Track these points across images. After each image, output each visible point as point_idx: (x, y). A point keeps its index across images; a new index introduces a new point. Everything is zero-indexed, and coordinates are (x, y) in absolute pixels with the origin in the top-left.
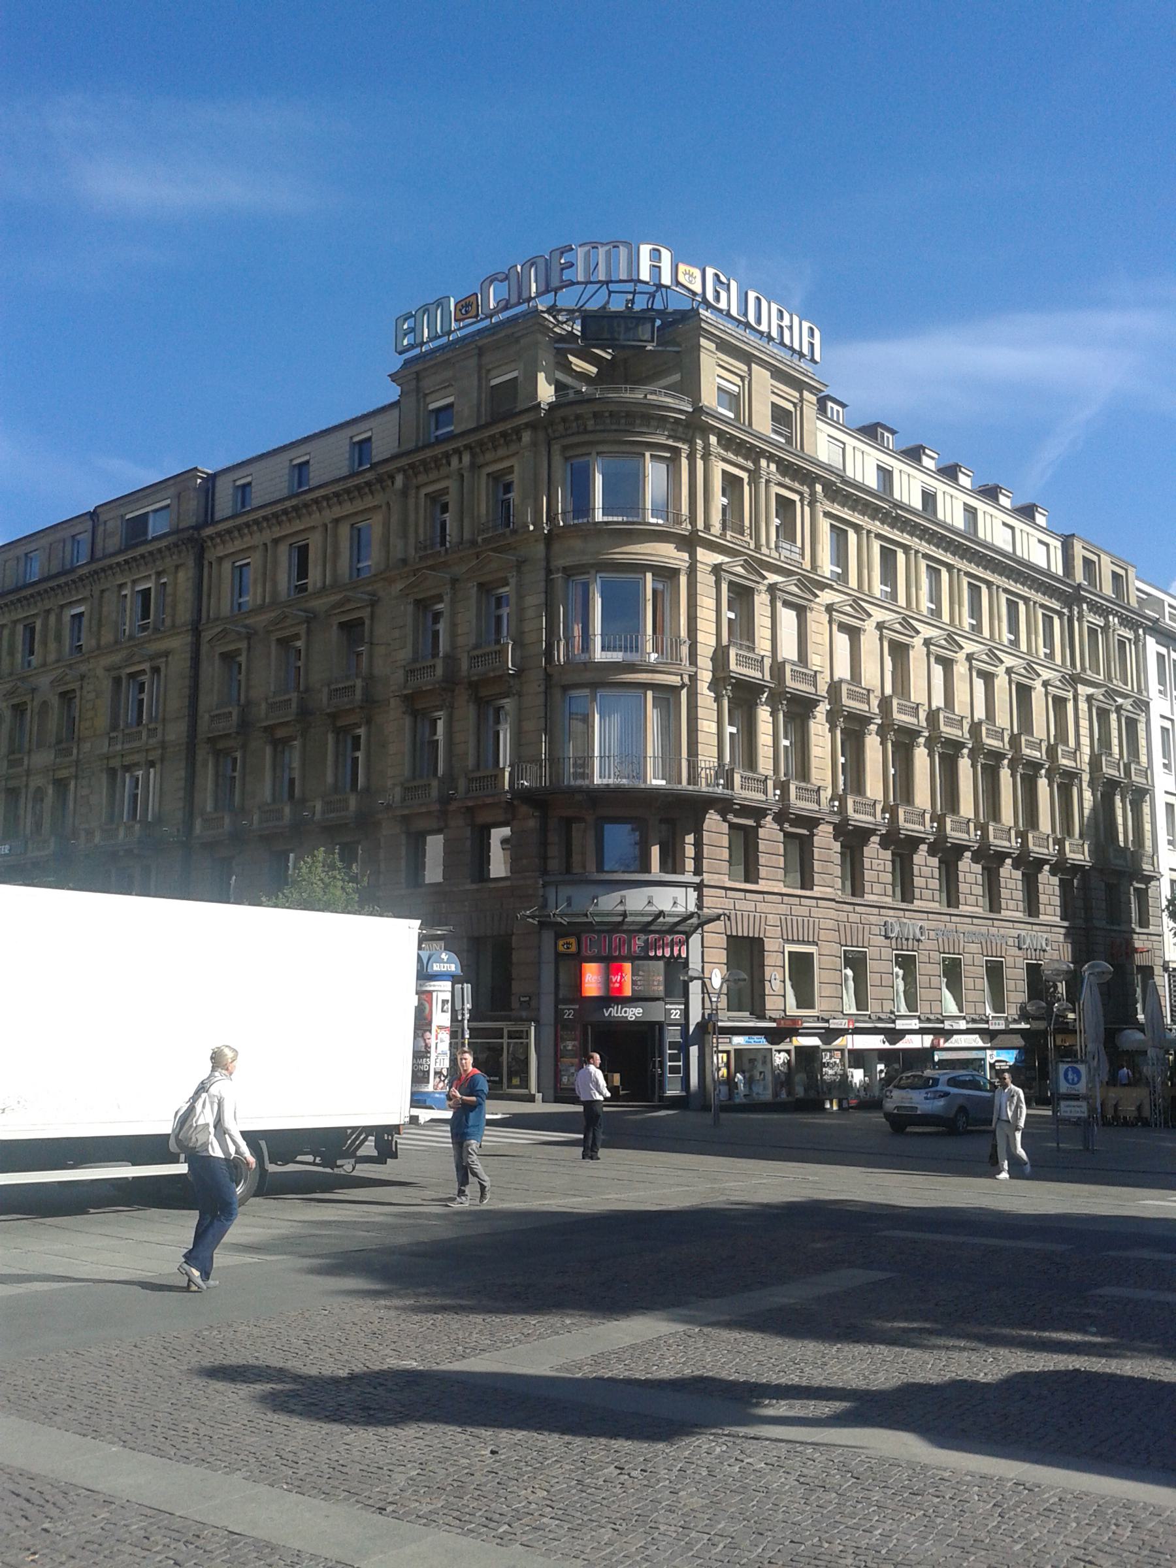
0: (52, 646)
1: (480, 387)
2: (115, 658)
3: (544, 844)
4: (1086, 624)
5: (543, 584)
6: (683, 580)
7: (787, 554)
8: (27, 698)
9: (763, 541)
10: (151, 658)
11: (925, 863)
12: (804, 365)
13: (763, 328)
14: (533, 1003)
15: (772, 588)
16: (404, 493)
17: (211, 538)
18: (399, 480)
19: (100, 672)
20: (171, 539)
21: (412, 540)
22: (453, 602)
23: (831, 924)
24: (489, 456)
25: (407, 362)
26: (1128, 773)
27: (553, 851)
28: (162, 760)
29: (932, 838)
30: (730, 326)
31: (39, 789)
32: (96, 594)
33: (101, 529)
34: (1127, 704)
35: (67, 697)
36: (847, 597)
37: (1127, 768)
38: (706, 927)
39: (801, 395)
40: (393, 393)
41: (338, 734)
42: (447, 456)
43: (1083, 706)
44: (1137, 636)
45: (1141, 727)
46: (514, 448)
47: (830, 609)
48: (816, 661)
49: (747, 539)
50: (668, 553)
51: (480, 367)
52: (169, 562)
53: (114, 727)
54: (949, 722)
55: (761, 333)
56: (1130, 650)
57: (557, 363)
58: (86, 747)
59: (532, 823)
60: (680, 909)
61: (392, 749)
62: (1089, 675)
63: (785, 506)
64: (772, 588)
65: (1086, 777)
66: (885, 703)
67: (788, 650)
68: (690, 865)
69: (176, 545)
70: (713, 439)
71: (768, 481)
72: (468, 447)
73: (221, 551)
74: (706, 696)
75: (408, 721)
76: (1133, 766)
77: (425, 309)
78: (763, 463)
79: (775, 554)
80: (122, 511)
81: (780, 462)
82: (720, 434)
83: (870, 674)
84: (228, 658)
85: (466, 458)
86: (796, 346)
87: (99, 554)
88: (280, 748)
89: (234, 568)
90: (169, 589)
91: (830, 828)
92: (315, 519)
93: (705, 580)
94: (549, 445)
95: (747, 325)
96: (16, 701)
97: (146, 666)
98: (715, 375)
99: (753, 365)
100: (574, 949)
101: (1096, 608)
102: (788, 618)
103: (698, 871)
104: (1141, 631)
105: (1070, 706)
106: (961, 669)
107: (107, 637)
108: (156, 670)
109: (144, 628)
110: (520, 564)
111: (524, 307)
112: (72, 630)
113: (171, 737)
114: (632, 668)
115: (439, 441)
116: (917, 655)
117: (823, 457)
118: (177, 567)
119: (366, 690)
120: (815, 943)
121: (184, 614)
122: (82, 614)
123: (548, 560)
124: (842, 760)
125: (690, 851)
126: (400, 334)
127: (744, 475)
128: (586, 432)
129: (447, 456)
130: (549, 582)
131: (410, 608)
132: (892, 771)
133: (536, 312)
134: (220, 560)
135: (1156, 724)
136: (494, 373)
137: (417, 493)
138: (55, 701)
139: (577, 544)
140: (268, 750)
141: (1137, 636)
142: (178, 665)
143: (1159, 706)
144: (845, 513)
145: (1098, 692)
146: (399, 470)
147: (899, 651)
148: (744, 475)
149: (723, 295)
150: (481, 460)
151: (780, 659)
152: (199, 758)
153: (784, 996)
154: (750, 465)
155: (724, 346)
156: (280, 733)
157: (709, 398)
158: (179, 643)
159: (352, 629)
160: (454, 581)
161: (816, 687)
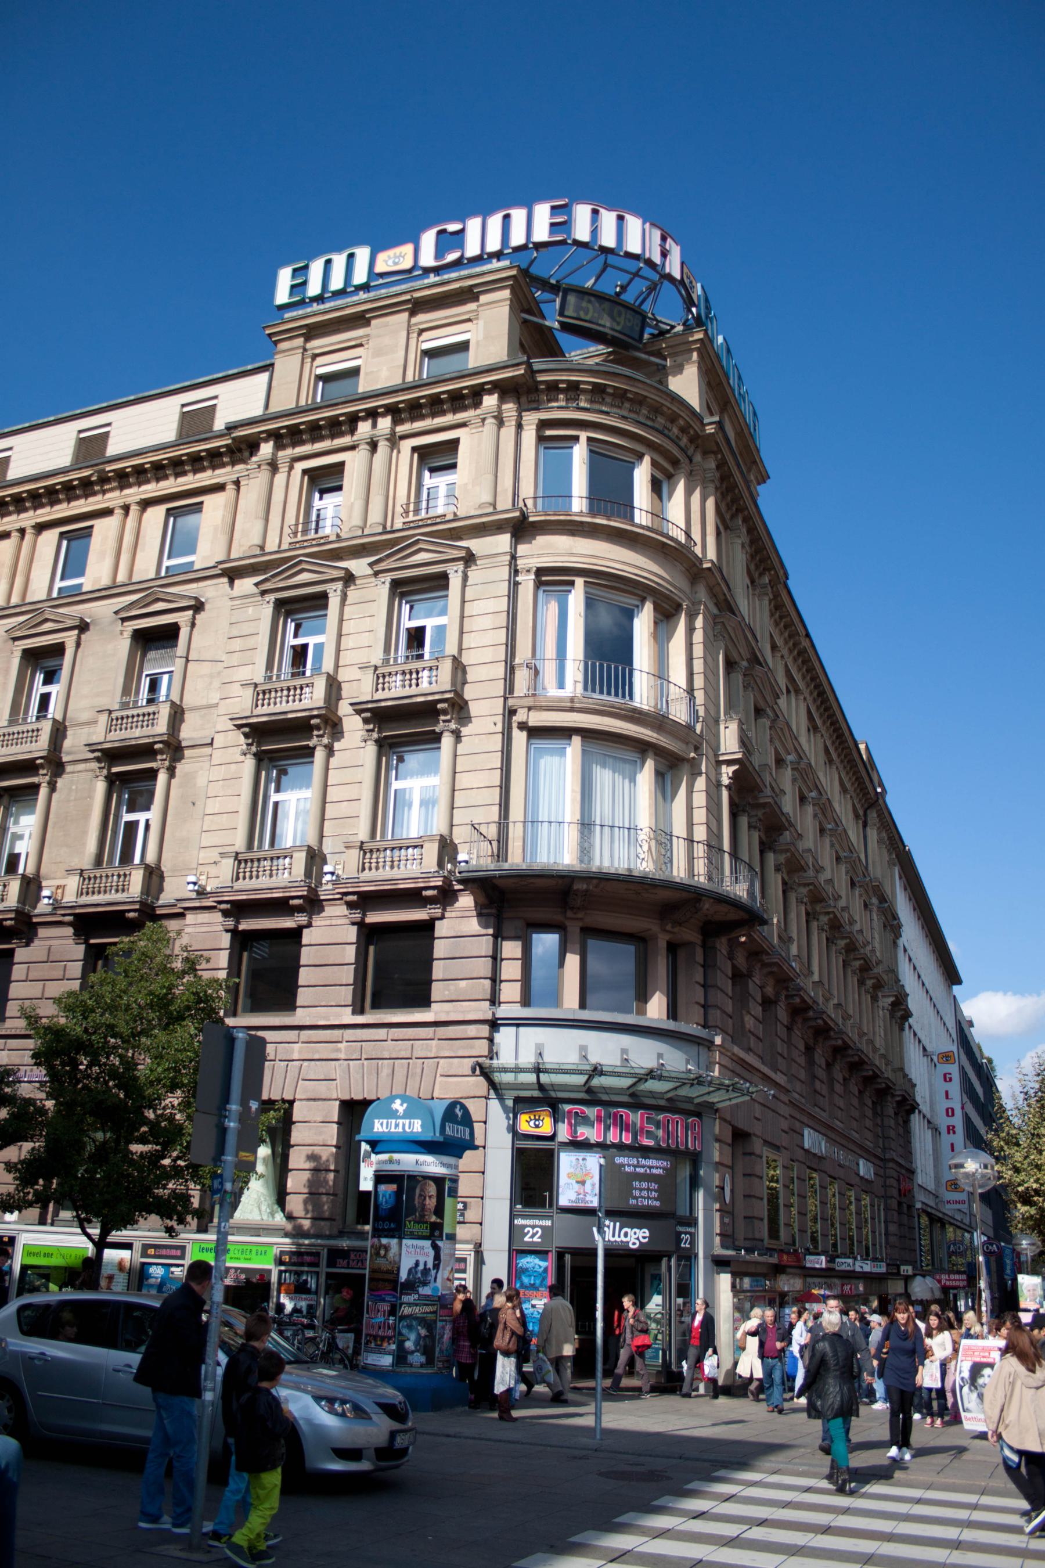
18: (266, 449)
85: (385, 423)
123: (514, 557)
129: (353, 420)
130: (514, 586)
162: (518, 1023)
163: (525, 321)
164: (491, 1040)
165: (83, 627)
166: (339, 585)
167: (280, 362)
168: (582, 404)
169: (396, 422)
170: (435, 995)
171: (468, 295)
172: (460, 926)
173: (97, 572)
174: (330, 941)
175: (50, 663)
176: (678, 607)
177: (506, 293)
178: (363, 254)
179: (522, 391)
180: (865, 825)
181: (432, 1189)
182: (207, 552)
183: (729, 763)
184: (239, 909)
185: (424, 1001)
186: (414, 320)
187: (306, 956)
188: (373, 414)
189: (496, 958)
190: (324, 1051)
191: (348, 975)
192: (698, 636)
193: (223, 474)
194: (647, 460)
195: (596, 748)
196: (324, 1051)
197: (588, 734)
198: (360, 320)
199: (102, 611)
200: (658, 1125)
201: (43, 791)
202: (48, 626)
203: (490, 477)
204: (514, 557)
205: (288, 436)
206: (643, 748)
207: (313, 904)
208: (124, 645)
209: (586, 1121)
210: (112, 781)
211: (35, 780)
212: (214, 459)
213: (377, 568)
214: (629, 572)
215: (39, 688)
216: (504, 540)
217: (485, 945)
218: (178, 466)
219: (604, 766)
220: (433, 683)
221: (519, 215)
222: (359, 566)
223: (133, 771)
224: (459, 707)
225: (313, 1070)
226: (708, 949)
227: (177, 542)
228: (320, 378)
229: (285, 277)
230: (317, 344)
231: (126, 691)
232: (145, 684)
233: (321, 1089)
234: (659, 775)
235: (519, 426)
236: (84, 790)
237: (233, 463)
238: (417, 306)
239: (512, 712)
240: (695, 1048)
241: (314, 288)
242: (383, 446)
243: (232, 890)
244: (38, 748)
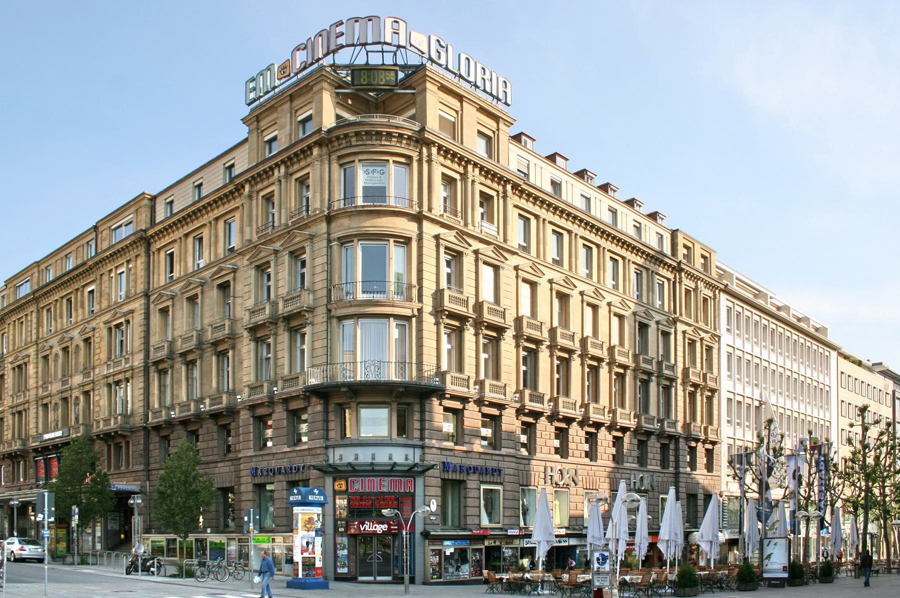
0: (80, 311)
1: (291, 122)
2: (107, 317)
3: (326, 421)
4: (683, 287)
6: (414, 245)
7: (489, 230)
8: (69, 344)
9: (470, 221)
10: (125, 314)
11: (576, 433)
12: (501, 106)
13: (472, 79)
15: (476, 252)
16: (250, 197)
17: (152, 236)
18: (247, 187)
19: (102, 325)
20: (133, 238)
21: (255, 227)
22: (276, 265)
23: (512, 472)
24: (296, 167)
25: (252, 111)
26: (705, 379)
27: (332, 425)
28: (132, 377)
29: (580, 418)
30: (450, 76)
31: (77, 398)
32: (99, 277)
33: (100, 236)
34: (707, 337)
35: (87, 341)
36: (527, 261)
37: (705, 376)
38: (427, 473)
39: (498, 126)
40: (243, 132)
41: (218, 356)
43: (680, 337)
44: (715, 295)
45: (715, 351)
46: (309, 160)
48: (507, 301)
49: (459, 219)
50: (408, 228)
51: (291, 108)
52: (132, 254)
53: (109, 359)
54: (594, 345)
55: (470, 82)
56: (710, 303)
58: (97, 371)
59: (319, 408)
60: (410, 462)
61: (245, 364)
62: (684, 318)
63: (486, 199)
64: (476, 252)
65: (679, 381)
66: (552, 331)
67: (487, 295)
68: (417, 434)
69: (135, 242)
70: (434, 150)
71: (473, 181)
72: (283, 162)
73: (158, 245)
74: (429, 320)
75: (253, 345)
76: (708, 375)
77: (261, 74)
80: (109, 224)
81: (482, 169)
82: (440, 148)
83: (543, 314)
84: (164, 311)
85: (283, 169)
86: (494, 93)
88: (190, 367)
89: (166, 255)
91: (514, 411)
92: (205, 219)
93: (429, 245)
94: (330, 156)
95: (461, 77)
96: (64, 345)
97: (122, 320)
98: (436, 108)
99: (464, 103)
100: (344, 488)
101: (690, 276)
102: (487, 273)
103: (422, 438)
104: (717, 291)
105: (672, 337)
106: (603, 312)
107: (105, 304)
110: (312, 237)
111: (316, 66)
112: (89, 300)
113: (136, 364)
114: (377, 304)
116: (575, 302)
117: (513, 168)
118: (137, 256)
119: (232, 328)
120: (501, 484)
122: (93, 291)
124: (556, 376)
125: (417, 425)
126: (248, 91)
127: (457, 176)
128: (351, 146)
130: (329, 247)
131: (253, 272)
132: (587, 383)
133: (322, 68)
134: (159, 250)
135: (724, 350)
136: (299, 112)
137: (257, 196)
138: (82, 344)
139: (345, 222)
140: (184, 368)
141: (715, 295)
142: (138, 319)
143: (726, 339)
144: (529, 206)
145: (689, 330)
146: (247, 181)
147: (563, 298)
148: (457, 176)
149: (443, 55)
150: (291, 170)
151: (480, 300)
152: (151, 374)
153: (479, 516)
154: (461, 170)
155: (443, 88)
156: (190, 357)
157: (432, 124)
159: (224, 287)
160: (276, 252)
161: (504, 318)
163: (338, 94)
169: (287, 167)
188: (277, 165)
243: (250, 401)
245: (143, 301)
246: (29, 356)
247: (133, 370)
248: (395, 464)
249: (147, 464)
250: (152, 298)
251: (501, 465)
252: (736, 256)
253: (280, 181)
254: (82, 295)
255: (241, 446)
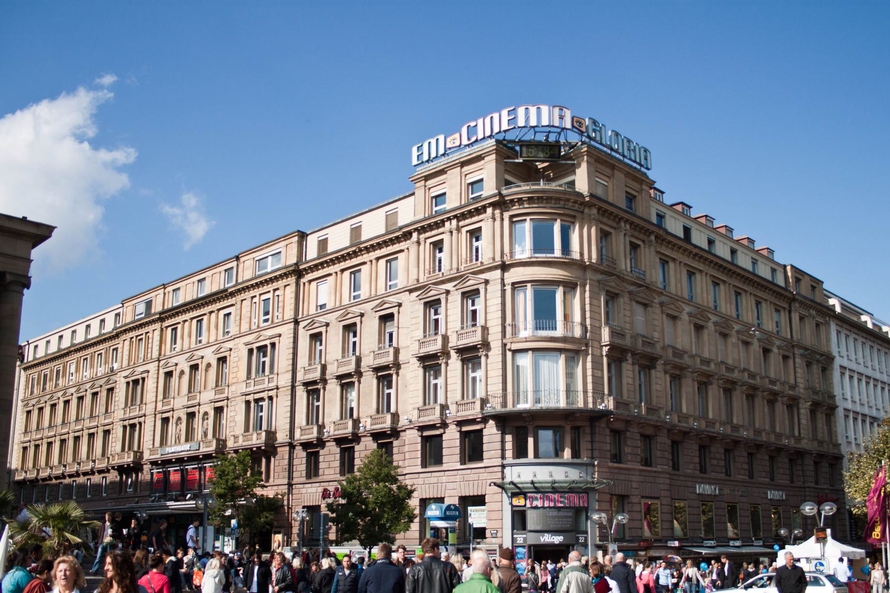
5: (500, 292)
8: (199, 362)
14: (499, 535)
16: (418, 243)
17: (305, 269)
18: (415, 235)
42: (443, 222)
47: (662, 304)
52: (280, 283)
57: (506, 170)
58: (232, 388)
61: (411, 388)
72: (455, 217)
78: (623, 224)
79: (630, 275)
85: (454, 222)
87: (240, 280)
90: (281, 298)
108: (273, 345)
109: (266, 321)
112: (749, 414)
115: (438, 213)
118: (285, 286)
121: (289, 314)
123: (503, 279)
129: (443, 222)
130: (503, 292)
134: (310, 281)
146: (416, 230)
158: (287, 331)
160: (448, 292)
162: (512, 465)
164: (503, 472)
165: (362, 315)
166: (444, 295)
167: (417, 192)
168: (526, 206)
169: (458, 221)
170: (484, 457)
171: (479, 158)
172: (491, 431)
173: (364, 293)
174: (451, 438)
175: (353, 329)
176: (577, 284)
177: (494, 156)
178: (441, 138)
179: (501, 204)
180: (790, 312)
181: (444, 531)
182: (401, 281)
183: (606, 346)
184: (421, 429)
185: (481, 459)
186: (463, 170)
187: (445, 444)
188: (449, 219)
189: (503, 442)
190: (452, 479)
191: (457, 450)
192: (587, 294)
193: (402, 245)
194: (559, 221)
195: (537, 354)
196: (452, 479)
197: (534, 350)
198: (442, 172)
199: (368, 307)
200: (565, 498)
201: (356, 384)
202: (350, 316)
203: (491, 246)
204: (503, 279)
205: (422, 230)
206: (560, 350)
207: (444, 425)
208: (377, 321)
209: (536, 499)
210: (378, 378)
211: (352, 380)
212: (398, 240)
213: (458, 287)
214: (549, 277)
215: (352, 339)
216: (499, 272)
217: (498, 437)
218: (386, 243)
219: (544, 360)
220: (475, 338)
221: (496, 116)
222: (449, 286)
223: (385, 376)
224: (486, 345)
225: (450, 486)
226: (592, 427)
227: (390, 275)
228: (432, 198)
229: (415, 152)
230: (430, 183)
231: (380, 341)
232: (387, 336)
233: (453, 493)
234: (567, 361)
235: (502, 219)
236: (369, 382)
237: (405, 241)
238: (463, 164)
239: (505, 345)
240: (585, 468)
241: (425, 157)
242: (455, 232)
244: (351, 368)
245: (292, 325)
246: (148, 372)
247: (277, 388)
248: (554, 482)
249: (290, 477)
250: (302, 325)
251: (415, 481)
252: (841, 288)
253: (451, 232)
254: (217, 318)
255: (407, 463)
